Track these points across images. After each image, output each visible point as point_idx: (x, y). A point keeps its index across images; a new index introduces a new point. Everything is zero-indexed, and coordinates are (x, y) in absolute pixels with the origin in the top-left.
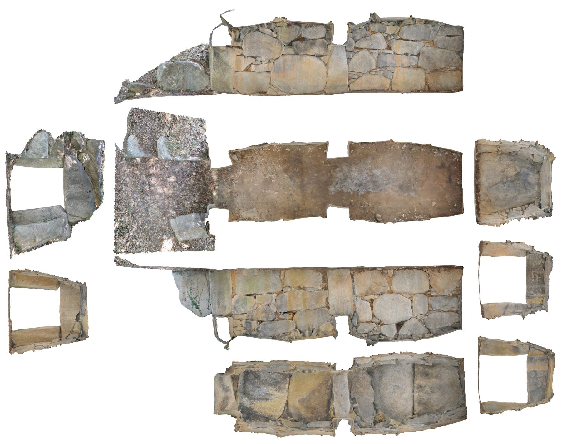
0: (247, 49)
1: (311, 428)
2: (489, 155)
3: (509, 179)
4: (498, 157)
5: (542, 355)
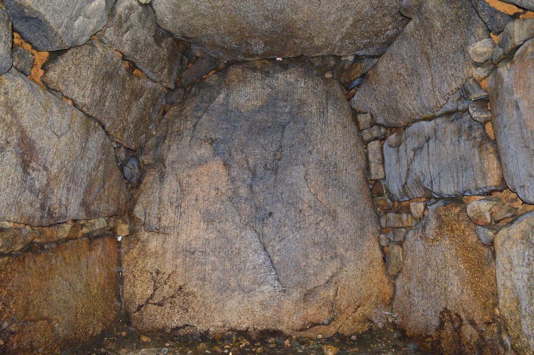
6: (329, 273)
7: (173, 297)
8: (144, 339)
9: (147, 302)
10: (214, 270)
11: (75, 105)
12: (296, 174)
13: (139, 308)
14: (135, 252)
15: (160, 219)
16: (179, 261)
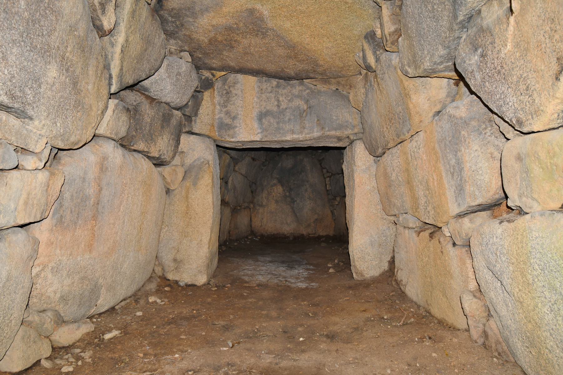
0: (409, 152)
1: (509, 346)
2: (254, 220)
3: (287, 194)
4: (258, 208)
5: (212, 97)
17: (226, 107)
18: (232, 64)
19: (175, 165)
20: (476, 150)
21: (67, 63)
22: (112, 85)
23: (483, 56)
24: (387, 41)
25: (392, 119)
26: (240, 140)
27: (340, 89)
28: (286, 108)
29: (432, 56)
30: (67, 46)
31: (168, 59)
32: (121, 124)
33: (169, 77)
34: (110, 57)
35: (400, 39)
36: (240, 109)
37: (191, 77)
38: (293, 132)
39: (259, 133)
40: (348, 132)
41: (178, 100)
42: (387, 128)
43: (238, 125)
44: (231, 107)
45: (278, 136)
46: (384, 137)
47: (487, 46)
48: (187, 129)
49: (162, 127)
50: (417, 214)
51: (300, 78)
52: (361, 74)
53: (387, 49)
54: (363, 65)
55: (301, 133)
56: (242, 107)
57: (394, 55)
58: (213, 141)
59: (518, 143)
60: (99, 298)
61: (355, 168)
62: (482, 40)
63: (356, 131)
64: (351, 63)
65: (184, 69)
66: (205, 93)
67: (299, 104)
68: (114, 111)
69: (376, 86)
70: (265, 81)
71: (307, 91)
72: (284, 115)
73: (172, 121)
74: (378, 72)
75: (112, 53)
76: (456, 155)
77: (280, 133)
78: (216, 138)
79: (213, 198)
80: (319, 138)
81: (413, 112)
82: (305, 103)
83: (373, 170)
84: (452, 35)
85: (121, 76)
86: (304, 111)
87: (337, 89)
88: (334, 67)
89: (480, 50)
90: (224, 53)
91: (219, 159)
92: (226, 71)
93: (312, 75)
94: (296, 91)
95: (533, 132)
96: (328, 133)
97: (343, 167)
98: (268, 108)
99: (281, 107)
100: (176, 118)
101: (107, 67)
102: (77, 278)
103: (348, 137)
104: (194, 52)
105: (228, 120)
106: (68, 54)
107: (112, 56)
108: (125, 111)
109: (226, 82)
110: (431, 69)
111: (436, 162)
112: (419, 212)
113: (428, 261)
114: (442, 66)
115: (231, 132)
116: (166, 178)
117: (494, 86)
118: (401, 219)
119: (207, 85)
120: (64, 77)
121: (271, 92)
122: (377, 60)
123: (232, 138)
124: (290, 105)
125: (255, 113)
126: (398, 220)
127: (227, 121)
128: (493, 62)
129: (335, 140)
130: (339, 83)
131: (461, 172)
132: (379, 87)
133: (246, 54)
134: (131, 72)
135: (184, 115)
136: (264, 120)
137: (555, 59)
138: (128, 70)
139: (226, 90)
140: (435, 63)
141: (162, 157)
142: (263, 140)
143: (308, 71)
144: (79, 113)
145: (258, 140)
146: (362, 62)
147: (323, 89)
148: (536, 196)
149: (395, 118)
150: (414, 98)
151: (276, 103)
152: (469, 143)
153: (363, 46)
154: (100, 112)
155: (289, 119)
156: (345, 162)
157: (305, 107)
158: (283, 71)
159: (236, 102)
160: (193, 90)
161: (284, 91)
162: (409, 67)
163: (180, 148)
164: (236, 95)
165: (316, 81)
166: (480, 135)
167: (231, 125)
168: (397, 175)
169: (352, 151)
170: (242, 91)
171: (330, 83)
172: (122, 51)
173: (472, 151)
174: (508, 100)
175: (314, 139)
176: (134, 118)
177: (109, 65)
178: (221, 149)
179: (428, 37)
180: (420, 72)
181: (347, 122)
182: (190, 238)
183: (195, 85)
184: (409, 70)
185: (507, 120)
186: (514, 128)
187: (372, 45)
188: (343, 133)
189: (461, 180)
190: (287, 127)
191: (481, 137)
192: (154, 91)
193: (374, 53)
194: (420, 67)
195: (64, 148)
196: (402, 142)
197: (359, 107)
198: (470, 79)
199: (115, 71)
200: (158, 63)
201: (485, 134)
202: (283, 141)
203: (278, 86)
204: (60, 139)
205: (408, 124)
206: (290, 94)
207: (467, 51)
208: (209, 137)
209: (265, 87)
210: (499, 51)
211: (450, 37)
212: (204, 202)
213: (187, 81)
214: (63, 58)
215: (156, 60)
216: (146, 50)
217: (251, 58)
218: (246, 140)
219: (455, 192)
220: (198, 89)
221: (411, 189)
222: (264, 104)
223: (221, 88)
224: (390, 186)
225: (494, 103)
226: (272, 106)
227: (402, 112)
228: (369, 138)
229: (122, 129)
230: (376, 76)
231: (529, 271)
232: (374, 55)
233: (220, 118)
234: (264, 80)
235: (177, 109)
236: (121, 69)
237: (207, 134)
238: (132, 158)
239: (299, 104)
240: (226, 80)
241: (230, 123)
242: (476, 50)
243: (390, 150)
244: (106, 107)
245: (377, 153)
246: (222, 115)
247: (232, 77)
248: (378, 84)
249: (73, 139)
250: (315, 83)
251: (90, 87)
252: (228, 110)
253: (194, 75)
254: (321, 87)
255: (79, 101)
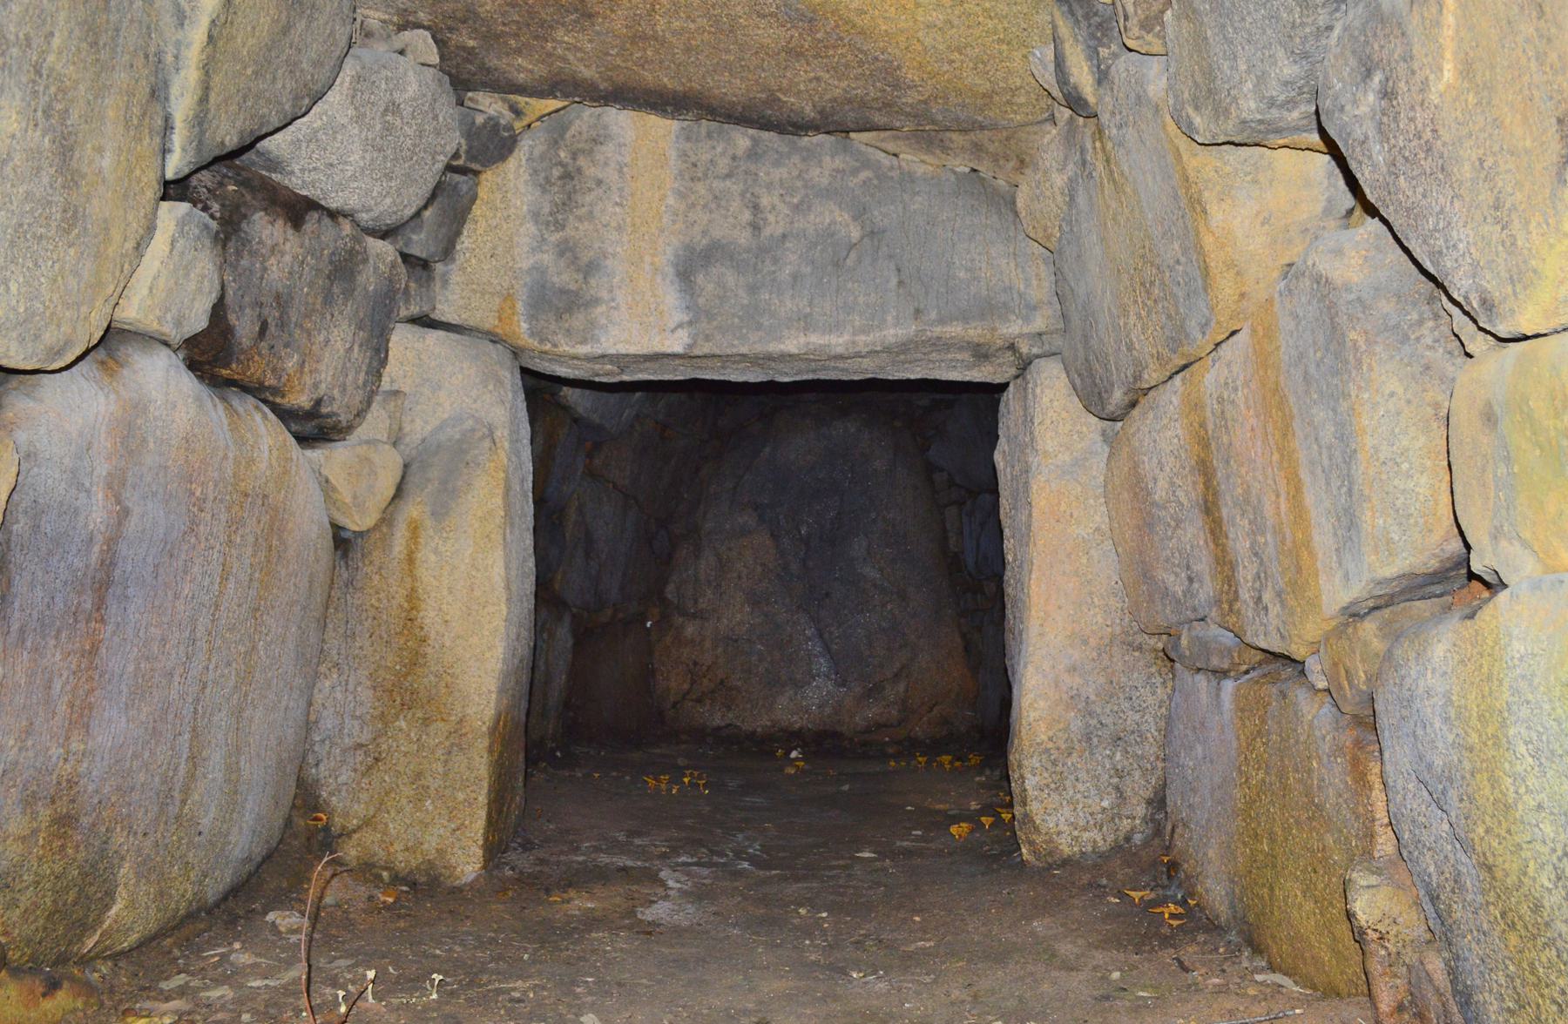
6: (898, 665)
7: (713, 692)
8: (684, 737)
9: (684, 698)
10: (760, 660)
11: (615, 486)
12: (858, 547)
13: (675, 705)
14: (668, 640)
15: (696, 602)
16: (720, 650)
17: (560, 226)
18: (587, 73)
19: (368, 442)
20: (1392, 394)
21: (47, 87)
22: (170, 151)
23: (1387, 94)
24: (1126, 18)
25: (1152, 283)
26: (612, 351)
27: (985, 169)
28: (784, 236)
29: (1262, 79)
30: (52, 34)
31: (358, 57)
32: (192, 286)
33: (359, 118)
34: (169, 59)
35: (1169, 13)
36: (614, 236)
37: (436, 117)
38: (806, 322)
39: (680, 326)
40: (1013, 328)
41: (388, 201)
42: (1139, 317)
43: (605, 295)
44: (577, 229)
45: (753, 337)
46: (1130, 348)
47: (1393, 65)
48: (414, 310)
49: (328, 300)
50: (1232, 619)
51: (834, 124)
52: (1052, 120)
53: (1130, 44)
54: (1056, 93)
55: (836, 327)
56: (619, 228)
57: (1154, 67)
58: (509, 355)
59: (1494, 368)
60: (113, 900)
61: (1034, 460)
62: (1382, 47)
63: (1039, 324)
64: (1018, 82)
65: (412, 89)
66: (483, 177)
67: (833, 222)
68: (173, 243)
69: (1100, 166)
70: (709, 135)
71: (864, 174)
72: (775, 261)
73: (361, 279)
74: (1105, 118)
75: (178, 44)
76: (1334, 410)
77: (759, 327)
78: (521, 343)
79: (507, 568)
80: (904, 347)
81: (1215, 261)
82: (855, 218)
83: (1098, 465)
84: (1310, 20)
85: (200, 120)
86: (852, 246)
87: (974, 170)
88: (959, 93)
89: (1377, 78)
90: (560, 34)
91: (532, 422)
92: (566, 96)
93: (879, 118)
94: (820, 175)
95: (1526, 338)
96: (938, 330)
97: (997, 457)
98: (717, 233)
99: (767, 232)
100: (376, 268)
101: (158, 93)
102: (45, 813)
103: (1012, 347)
104: (450, 29)
105: (565, 277)
106: (51, 58)
107: (176, 57)
108: (208, 242)
109: (562, 136)
110: (1261, 122)
111: (1285, 435)
112: (1239, 612)
113: (1263, 781)
114: (1296, 114)
115: (578, 321)
116: (334, 489)
117: (1420, 190)
118: (1184, 642)
119: (491, 146)
120: (38, 133)
121: (729, 176)
122: (1102, 77)
123: (584, 342)
124: (800, 223)
125: (669, 250)
126: (1176, 646)
127: (564, 278)
128: (1411, 114)
129: (966, 356)
130: (978, 148)
131: (1348, 464)
132: (1111, 172)
133: (638, 38)
134: (234, 107)
135: (405, 257)
136: (700, 278)
137: (1554, 120)
138: (225, 101)
139: (561, 164)
140: (1272, 103)
141: (324, 410)
142: (697, 352)
143: (863, 104)
144: (72, 251)
145: (679, 349)
146: (1053, 81)
147: (920, 170)
148: (1527, 535)
149: (1163, 283)
150: (1217, 214)
151: (747, 216)
152: (1371, 369)
153: (1055, 28)
154: (130, 245)
155: (795, 277)
156: (1002, 441)
157: (855, 234)
158: (772, 100)
159: (597, 213)
160: (440, 166)
161: (780, 173)
162: (1197, 108)
163: (385, 379)
164: (599, 182)
165: (896, 138)
166: (1402, 343)
167: (576, 294)
168: (1172, 484)
169: (1026, 397)
170: (620, 171)
171: (945, 149)
172: (210, 37)
173: (1378, 399)
174: (1454, 233)
175: (887, 350)
176: (234, 267)
177: (166, 85)
178: (541, 390)
179: (1243, 19)
180: (1229, 129)
181: (1009, 289)
182: (420, 714)
183: (450, 149)
184: (1197, 120)
185: (1455, 296)
186: (1475, 322)
187: (1084, 24)
188: (994, 329)
189: (1350, 492)
190: (789, 305)
191: (1407, 349)
192: (303, 170)
193: (1093, 54)
194: (1227, 111)
195: (22, 366)
196: (1185, 367)
197: (1048, 238)
198: (1360, 163)
199: (182, 106)
200: (323, 75)
201: (1418, 339)
202: (770, 358)
203: (753, 154)
204: (14, 335)
205: (1202, 305)
206: (799, 184)
207: (1345, 74)
208: (494, 338)
209: (706, 157)
210: (1425, 87)
211: (1303, 24)
212: (473, 592)
213: (420, 133)
214: (39, 73)
215: (317, 64)
216: (286, 30)
217: (657, 52)
218: (633, 350)
219: (1335, 534)
220: (460, 162)
221: (1216, 530)
222: (702, 217)
223: (542, 157)
224: (1151, 526)
225: (1425, 241)
226: (732, 227)
227: (1183, 260)
228: (1081, 354)
229: (197, 305)
230: (1100, 131)
231: (1507, 765)
232: (1090, 58)
233: (539, 269)
234: (703, 131)
235: (386, 234)
236: (204, 99)
237: (487, 326)
238: (220, 407)
239: (833, 222)
240: (563, 129)
241: (573, 287)
242: (1368, 74)
243: (1151, 393)
244: (151, 229)
245: (1113, 403)
246: (547, 258)
247: (586, 117)
248: (1108, 161)
249: (50, 337)
250: (891, 147)
251: (107, 162)
252: (566, 241)
253: (447, 110)
254: (916, 161)
255: (76, 212)
